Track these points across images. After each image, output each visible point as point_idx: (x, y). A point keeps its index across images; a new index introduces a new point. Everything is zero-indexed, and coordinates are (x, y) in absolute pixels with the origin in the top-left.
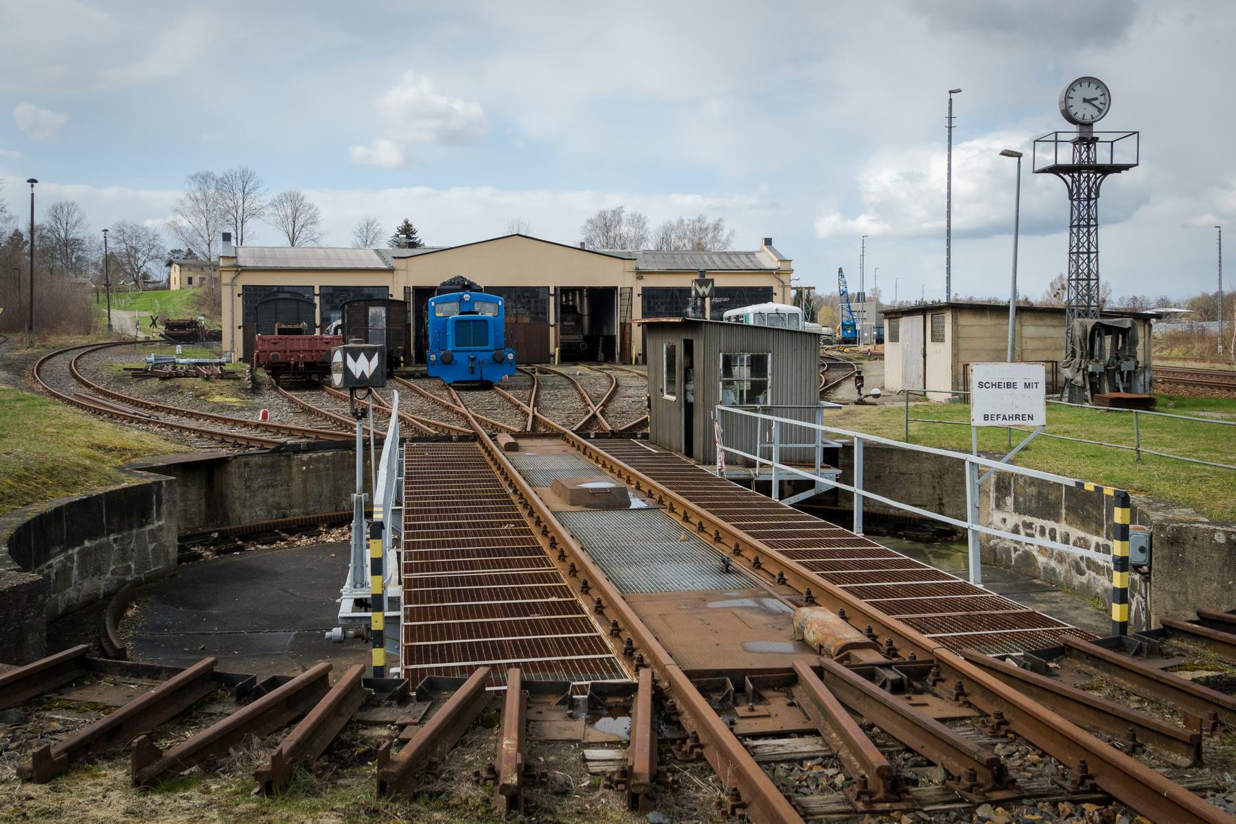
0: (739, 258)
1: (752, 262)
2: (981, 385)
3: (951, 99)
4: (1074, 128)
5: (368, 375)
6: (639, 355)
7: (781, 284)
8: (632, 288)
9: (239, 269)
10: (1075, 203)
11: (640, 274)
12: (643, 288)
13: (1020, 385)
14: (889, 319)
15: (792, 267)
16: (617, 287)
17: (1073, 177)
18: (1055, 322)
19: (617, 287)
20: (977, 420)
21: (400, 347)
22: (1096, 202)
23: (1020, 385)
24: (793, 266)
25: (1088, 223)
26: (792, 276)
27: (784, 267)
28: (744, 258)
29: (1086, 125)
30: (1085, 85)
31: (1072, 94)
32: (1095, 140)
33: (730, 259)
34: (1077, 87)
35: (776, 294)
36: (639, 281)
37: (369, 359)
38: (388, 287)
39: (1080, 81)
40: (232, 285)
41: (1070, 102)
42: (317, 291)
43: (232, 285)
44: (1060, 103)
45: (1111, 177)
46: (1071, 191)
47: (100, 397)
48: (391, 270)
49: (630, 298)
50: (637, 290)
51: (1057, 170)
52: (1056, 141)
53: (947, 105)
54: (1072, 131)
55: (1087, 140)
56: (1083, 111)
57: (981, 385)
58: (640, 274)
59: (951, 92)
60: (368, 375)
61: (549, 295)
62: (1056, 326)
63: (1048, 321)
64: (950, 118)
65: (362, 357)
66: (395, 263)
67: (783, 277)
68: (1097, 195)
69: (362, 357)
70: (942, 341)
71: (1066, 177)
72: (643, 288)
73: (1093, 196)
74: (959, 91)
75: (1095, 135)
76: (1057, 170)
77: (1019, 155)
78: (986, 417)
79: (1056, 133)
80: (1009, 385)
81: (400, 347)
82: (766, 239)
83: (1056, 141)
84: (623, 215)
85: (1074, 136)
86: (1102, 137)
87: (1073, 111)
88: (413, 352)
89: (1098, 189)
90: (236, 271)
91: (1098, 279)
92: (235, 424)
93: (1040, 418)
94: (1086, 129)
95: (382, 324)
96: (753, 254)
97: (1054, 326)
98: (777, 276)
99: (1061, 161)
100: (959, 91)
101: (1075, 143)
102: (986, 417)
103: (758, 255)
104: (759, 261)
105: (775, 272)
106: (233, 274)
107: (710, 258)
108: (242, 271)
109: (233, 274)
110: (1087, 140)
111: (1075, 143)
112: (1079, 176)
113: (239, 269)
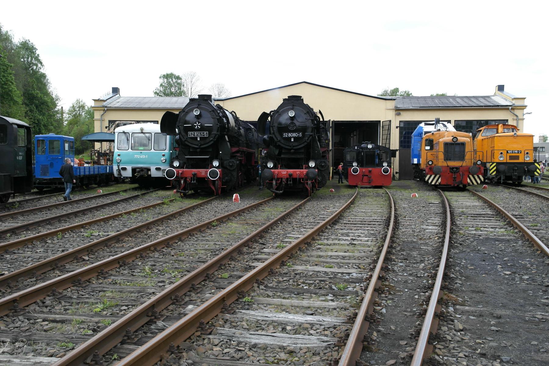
1: (489, 102)
6: (397, 173)
7: (515, 118)
8: (390, 121)
9: (106, 109)
11: (398, 111)
12: (400, 122)
15: (526, 104)
16: (380, 121)
19: (380, 121)
21: (356, 148)
24: (526, 103)
26: (525, 111)
27: (517, 103)
28: (482, 100)
33: (471, 100)
36: (397, 117)
40: (102, 120)
43: (102, 120)
47: (101, 191)
49: (389, 129)
50: (395, 123)
58: (398, 111)
62: (261, 204)
67: (517, 112)
70: (510, 160)
72: (400, 122)
81: (356, 148)
88: (38, 197)
90: (104, 110)
92: (163, 221)
96: (488, 97)
98: (512, 111)
105: (510, 108)
106: (102, 112)
108: (107, 110)
109: (102, 112)
113: (106, 109)
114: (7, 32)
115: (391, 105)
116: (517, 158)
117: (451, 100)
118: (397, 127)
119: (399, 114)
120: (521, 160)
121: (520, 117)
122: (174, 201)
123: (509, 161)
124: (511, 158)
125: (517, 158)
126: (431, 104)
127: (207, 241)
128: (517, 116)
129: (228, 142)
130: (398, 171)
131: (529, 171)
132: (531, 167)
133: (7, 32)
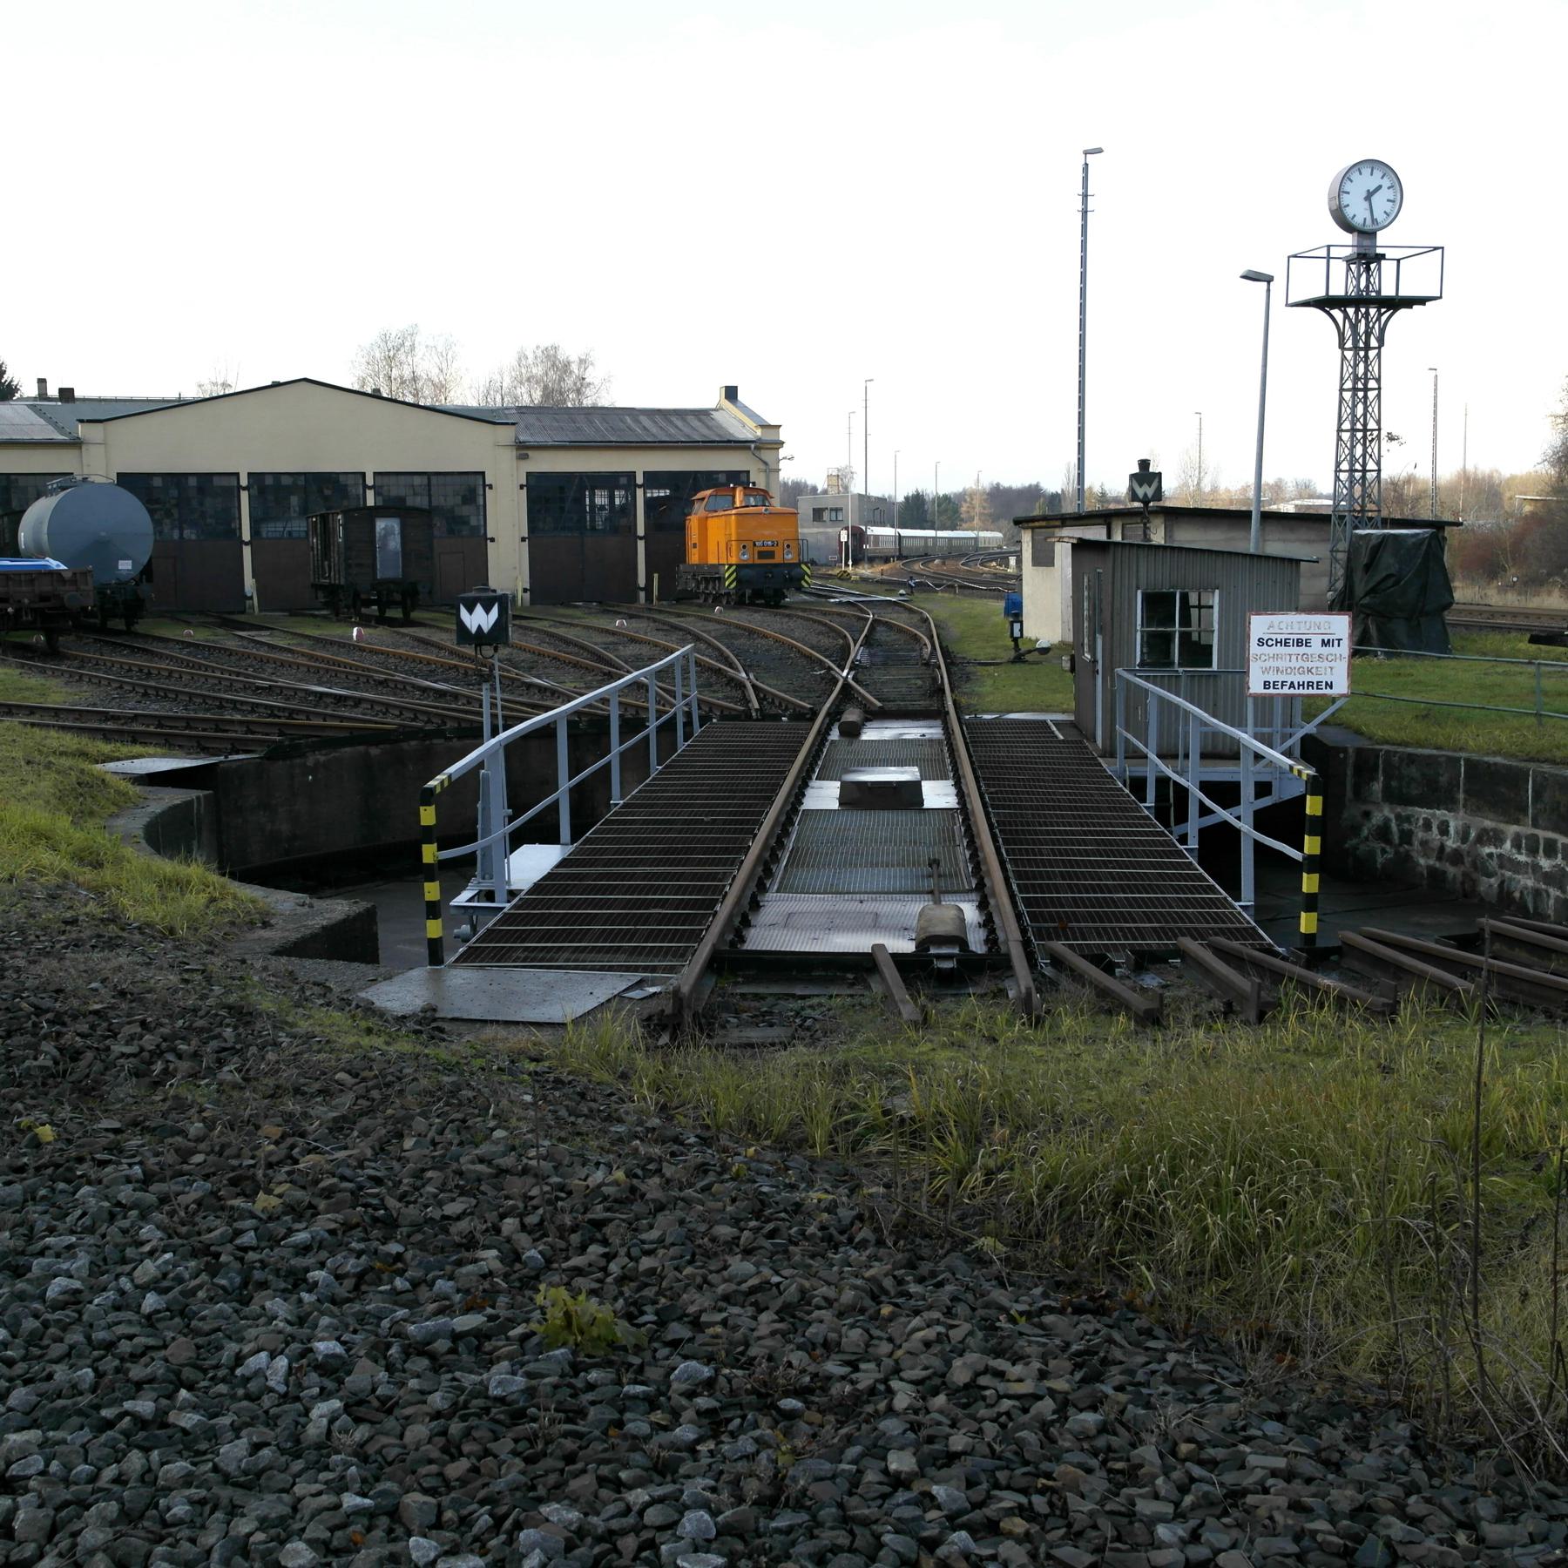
0: (684, 420)
1: (709, 427)
2: (1261, 642)
3: (1086, 166)
4: (1348, 238)
5: (486, 629)
7: (762, 467)
10: (1349, 354)
11: (523, 449)
12: (529, 474)
13: (1316, 641)
14: (1033, 528)
15: (782, 438)
17: (1346, 316)
18: (1312, 535)
20: (1256, 686)
22: (1379, 355)
23: (1316, 641)
25: (1365, 384)
26: (782, 452)
27: (769, 436)
28: (695, 423)
29: (1366, 234)
30: (1366, 171)
31: (1348, 186)
32: (1383, 257)
34: (1355, 176)
35: (492, 540)
37: (488, 610)
38: (483, 474)
39: (1358, 166)
41: (1346, 199)
42: (244, 482)
44: (1330, 199)
45: (1403, 312)
46: (1341, 335)
48: (76, 444)
51: (1325, 303)
52: (1329, 258)
53: (1080, 175)
54: (1345, 242)
55: (1367, 258)
56: (1357, 212)
57: (1261, 642)
59: (1086, 153)
60: (486, 629)
61: (365, 487)
63: (1304, 532)
64: (1085, 196)
65: (479, 609)
66: (81, 430)
67: (766, 455)
68: (1381, 341)
69: (479, 609)
71: (1337, 313)
72: (529, 474)
73: (1374, 343)
74: (1100, 151)
75: (1379, 251)
76: (1325, 303)
77: (1269, 280)
78: (1266, 685)
79: (1329, 247)
80: (1299, 643)
82: (727, 388)
83: (1329, 258)
84: (418, 339)
85: (1348, 252)
86: (1389, 253)
87: (1349, 212)
89: (1382, 331)
91: (1379, 471)
93: (1341, 686)
94: (1366, 242)
95: (395, 543)
97: (1309, 541)
99: (1337, 290)
100: (1100, 151)
101: (1349, 261)
102: (1266, 685)
103: (715, 415)
104: (720, 427)
107: (638, 422)
110: (1367, 258)
111: (1349, 261)
112: (1356, 313)
114: (1145, 475)
115: (506, 435)
116: (771, 555)
117: (628, 420)
118: (522, 487)
119: (523, 457)
120: (777, 560)
121: (772, 466)
122: (1538, 1223)
123: (758, 561)
124: (762, 555)
125: (771, 555)
126: (590, 434)
127: (1365, 1252)
128: (766, 463)
129: (243, 543)
130: (524, 482)
131: (791, 579)
132: (795, 572)
133: (1145, 475)
